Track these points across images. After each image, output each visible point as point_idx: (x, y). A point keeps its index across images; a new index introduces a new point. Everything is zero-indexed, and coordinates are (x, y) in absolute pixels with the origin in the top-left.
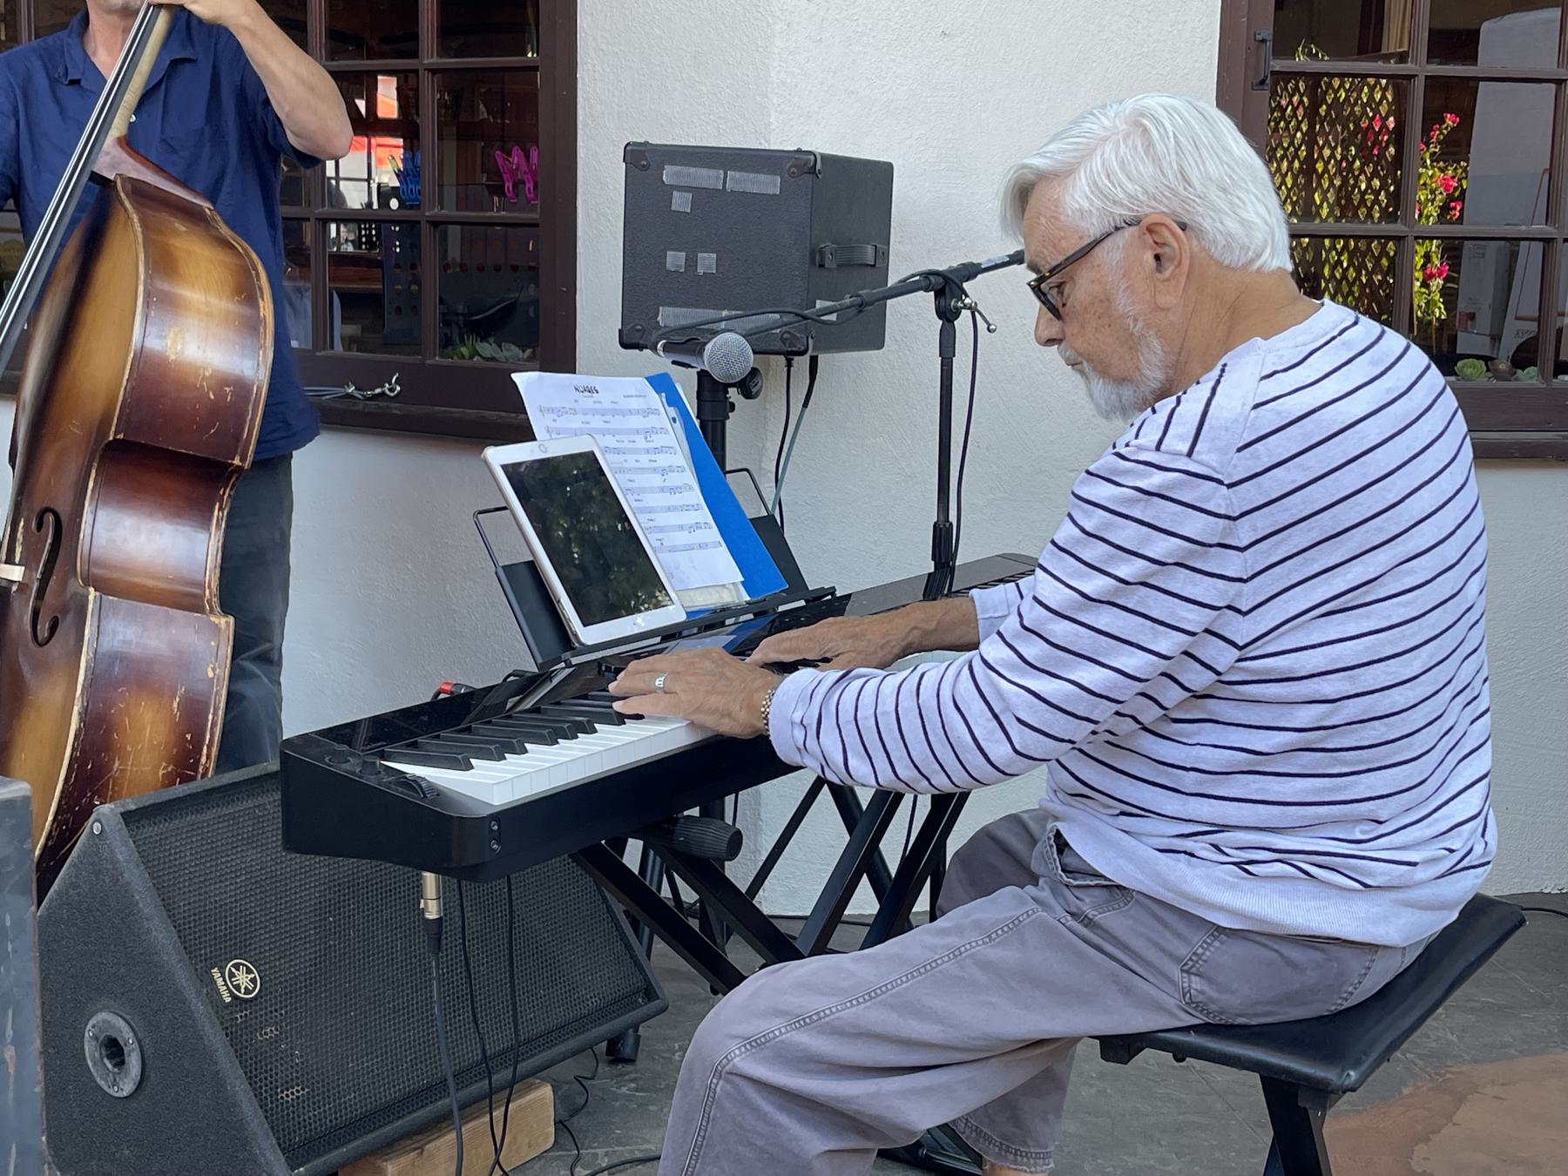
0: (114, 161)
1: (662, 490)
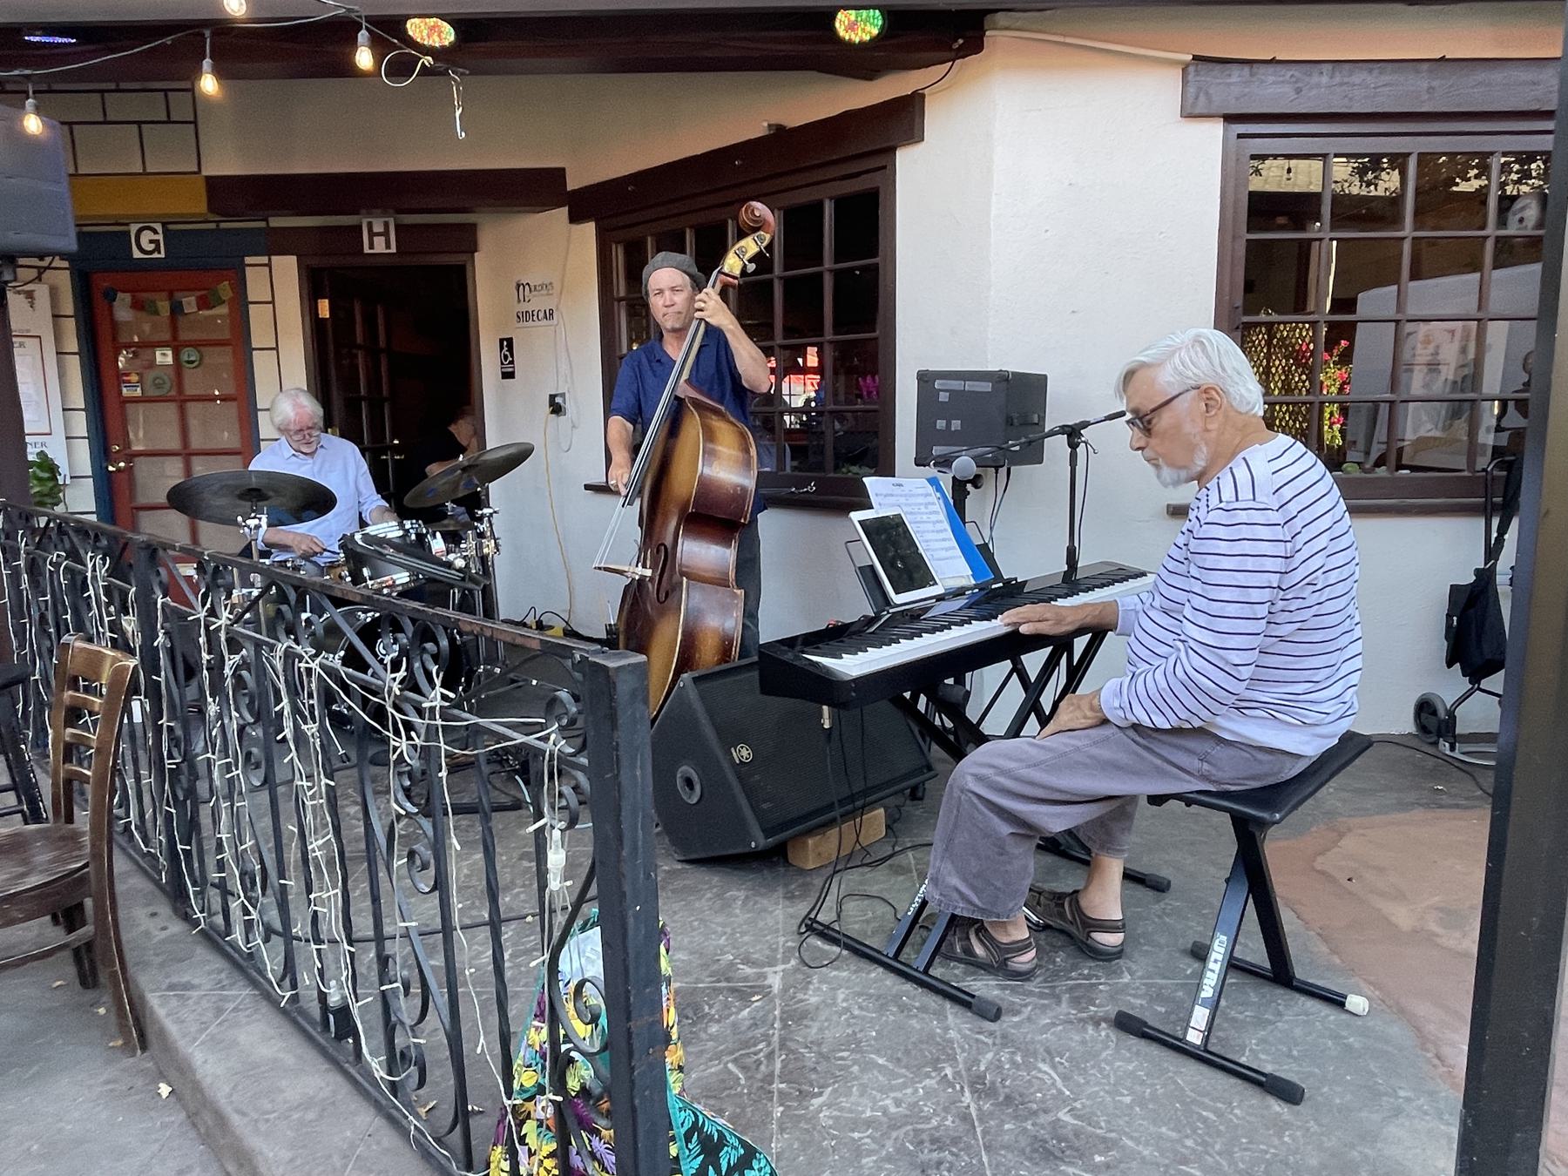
0: (685, 391)
1: (933, 531)
